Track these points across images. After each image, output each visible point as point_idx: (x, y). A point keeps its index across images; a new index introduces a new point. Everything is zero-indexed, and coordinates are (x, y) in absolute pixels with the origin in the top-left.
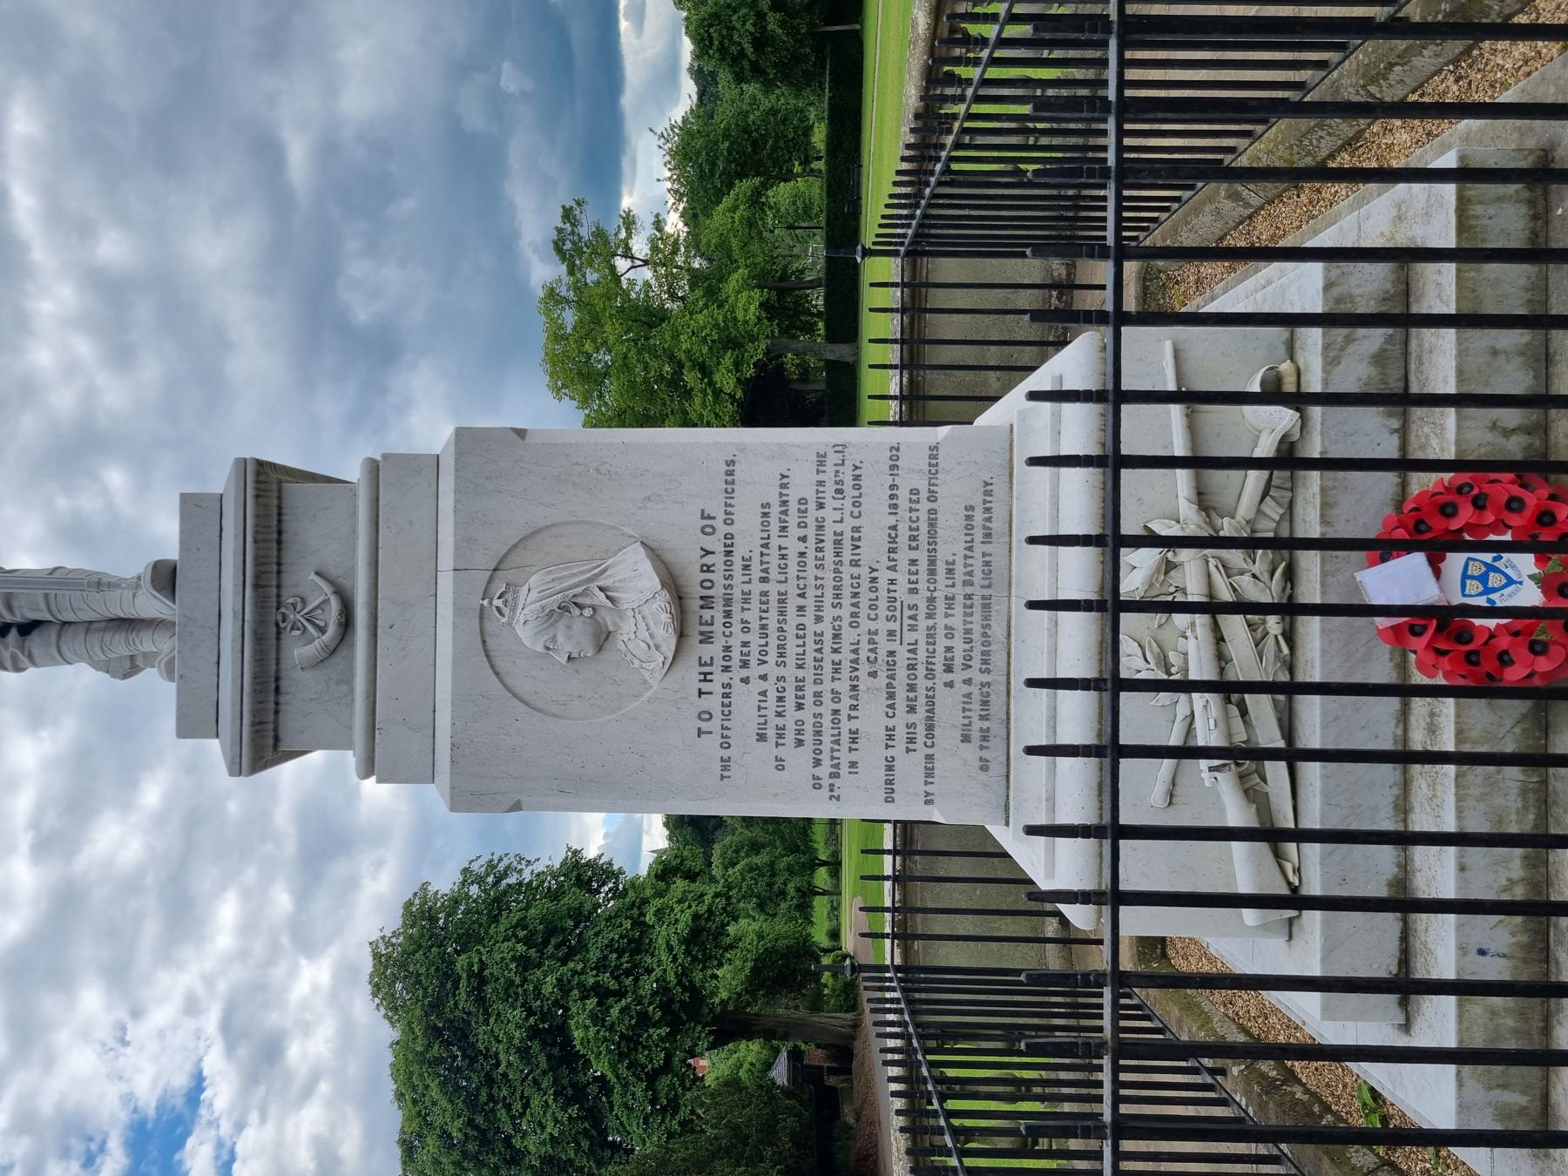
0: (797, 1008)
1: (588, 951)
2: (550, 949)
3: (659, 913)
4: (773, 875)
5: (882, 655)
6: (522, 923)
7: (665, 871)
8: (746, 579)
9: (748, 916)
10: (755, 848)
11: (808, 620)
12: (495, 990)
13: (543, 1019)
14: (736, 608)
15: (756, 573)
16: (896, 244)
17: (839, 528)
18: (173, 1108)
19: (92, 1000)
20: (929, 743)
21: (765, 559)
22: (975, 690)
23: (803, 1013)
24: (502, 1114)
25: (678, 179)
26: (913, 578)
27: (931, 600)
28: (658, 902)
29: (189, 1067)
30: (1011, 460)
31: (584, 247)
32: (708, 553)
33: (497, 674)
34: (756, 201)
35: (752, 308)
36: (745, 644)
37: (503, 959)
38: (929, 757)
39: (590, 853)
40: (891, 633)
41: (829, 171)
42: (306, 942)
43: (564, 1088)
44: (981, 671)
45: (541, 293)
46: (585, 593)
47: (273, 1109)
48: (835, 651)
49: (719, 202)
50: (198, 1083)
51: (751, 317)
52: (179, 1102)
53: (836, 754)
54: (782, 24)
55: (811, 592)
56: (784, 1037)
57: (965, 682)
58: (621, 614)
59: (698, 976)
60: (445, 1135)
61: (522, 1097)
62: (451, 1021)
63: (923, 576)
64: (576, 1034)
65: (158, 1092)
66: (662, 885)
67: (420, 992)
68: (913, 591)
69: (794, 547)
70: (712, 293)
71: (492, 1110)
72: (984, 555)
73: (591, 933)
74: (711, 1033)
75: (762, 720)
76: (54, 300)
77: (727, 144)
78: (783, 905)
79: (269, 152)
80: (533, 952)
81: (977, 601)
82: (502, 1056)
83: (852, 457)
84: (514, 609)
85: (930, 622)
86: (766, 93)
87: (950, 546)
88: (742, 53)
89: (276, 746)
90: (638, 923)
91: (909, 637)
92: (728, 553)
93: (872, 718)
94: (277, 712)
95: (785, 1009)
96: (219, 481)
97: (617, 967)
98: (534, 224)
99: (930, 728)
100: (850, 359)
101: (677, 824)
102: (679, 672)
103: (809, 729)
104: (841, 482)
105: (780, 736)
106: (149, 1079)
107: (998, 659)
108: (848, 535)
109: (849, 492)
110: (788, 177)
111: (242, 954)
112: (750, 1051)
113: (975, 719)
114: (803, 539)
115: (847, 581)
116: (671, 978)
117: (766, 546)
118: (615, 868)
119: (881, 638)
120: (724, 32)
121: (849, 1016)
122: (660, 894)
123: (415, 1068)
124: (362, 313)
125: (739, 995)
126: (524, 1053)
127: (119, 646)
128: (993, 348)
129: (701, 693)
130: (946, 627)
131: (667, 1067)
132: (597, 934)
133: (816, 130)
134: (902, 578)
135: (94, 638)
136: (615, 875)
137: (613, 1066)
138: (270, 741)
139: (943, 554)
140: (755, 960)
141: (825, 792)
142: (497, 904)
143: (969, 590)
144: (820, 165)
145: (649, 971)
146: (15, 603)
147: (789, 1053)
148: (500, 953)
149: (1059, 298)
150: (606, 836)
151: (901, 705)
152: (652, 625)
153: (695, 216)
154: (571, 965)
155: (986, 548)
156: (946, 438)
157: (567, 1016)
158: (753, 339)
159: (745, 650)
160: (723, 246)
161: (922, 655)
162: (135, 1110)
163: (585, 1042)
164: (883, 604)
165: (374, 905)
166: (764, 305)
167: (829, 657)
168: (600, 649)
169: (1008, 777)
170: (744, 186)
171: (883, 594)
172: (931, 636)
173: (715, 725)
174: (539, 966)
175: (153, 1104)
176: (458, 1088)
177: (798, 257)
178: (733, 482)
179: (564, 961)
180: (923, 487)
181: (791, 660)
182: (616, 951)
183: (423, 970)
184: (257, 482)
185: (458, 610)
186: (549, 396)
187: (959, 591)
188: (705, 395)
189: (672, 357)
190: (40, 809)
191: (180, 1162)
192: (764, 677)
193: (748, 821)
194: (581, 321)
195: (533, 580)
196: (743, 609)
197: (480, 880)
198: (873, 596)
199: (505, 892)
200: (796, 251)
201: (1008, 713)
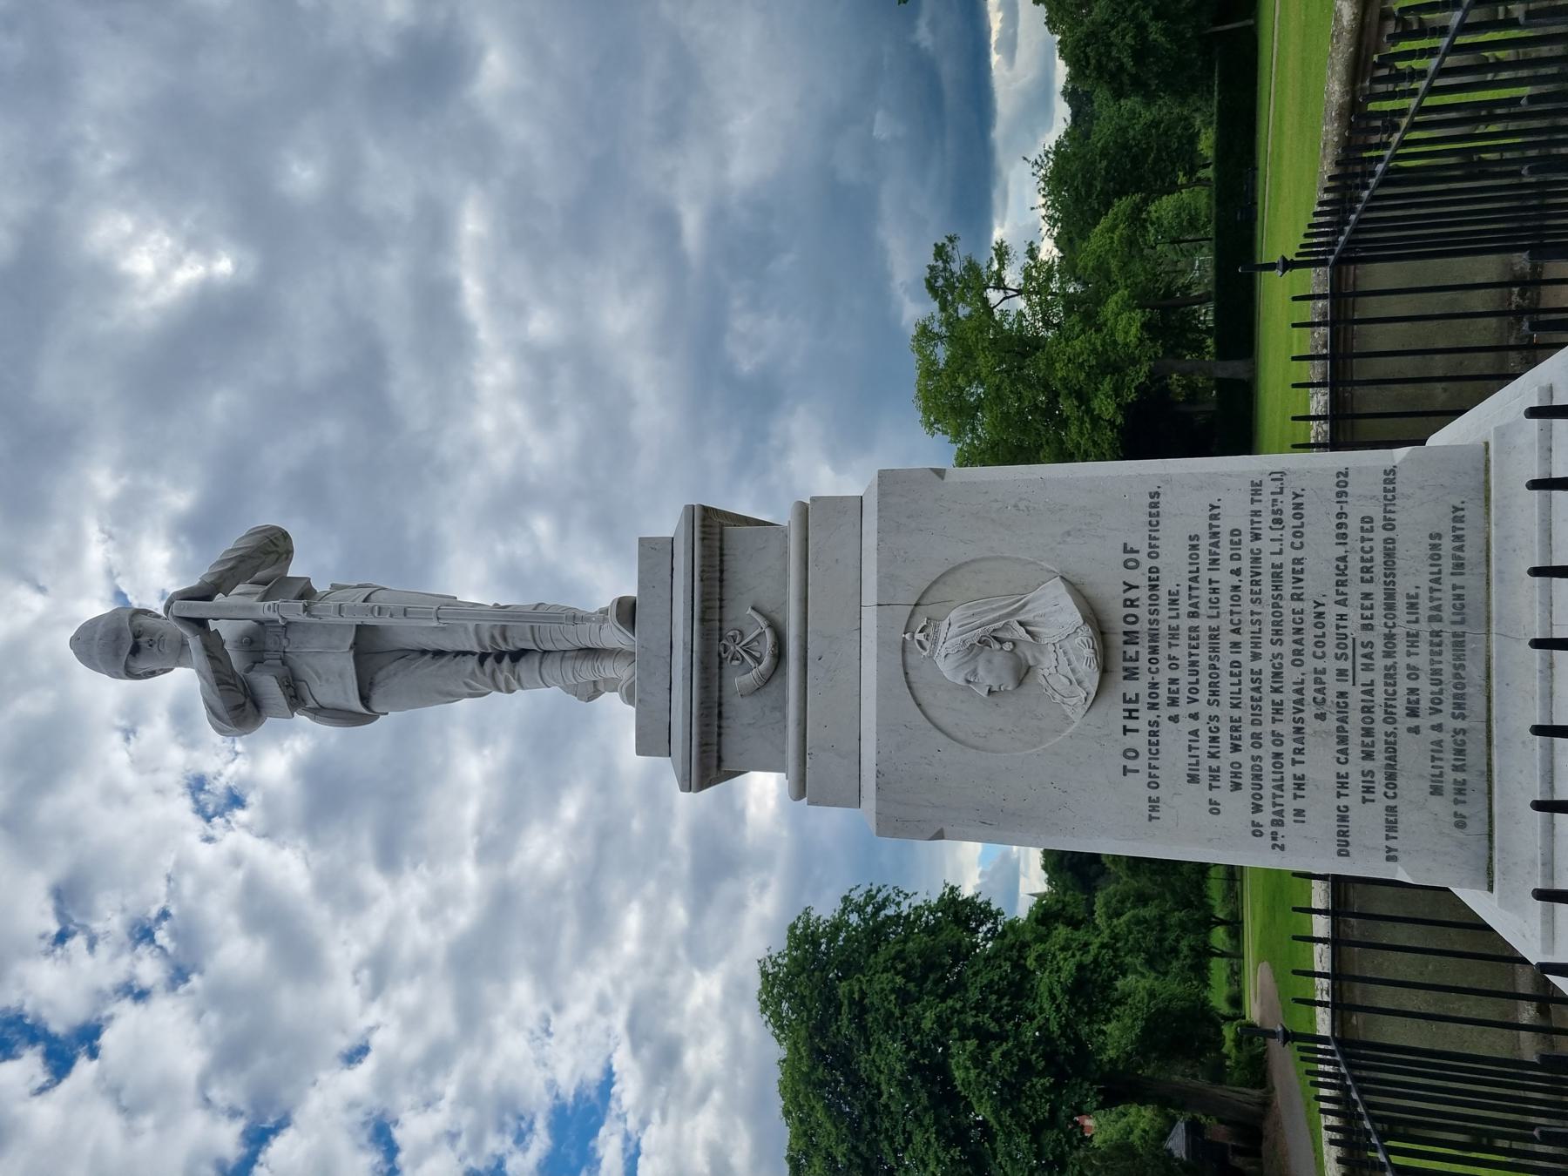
0: (1195, 1076)
1: (966, 990)
2: (929, 985)
3: (1040, 958)
4: (1164, 929)
5: (1331, 697)
6: (900, 956)
7: (1046, 915)
8: (1174, 613)
9: (1136, 972)
10: (1142, 899)
11: (1244, 656)
12: (876, 1019)
13: (925, 1053)
14: (1163, 644)
15: (1184, 606)
16: (1324, 253)
17: (1277, 560)
18: (588, 1098)
19: (522, 991)
20: (1390, 793)
21: (1194, 593)
22: (1447, 737)
23: (1202, 1082)
24: (885, 1145)
25: (1053, 205)
26: (1368, 613)
27: (1390, 637)
28: (1039, 948)
29: (601, 1061)
30: (1487, 482)
31: (956, 282)
32: (1131, 587)
33: (919, 705)
34: (1136, 218)
35: (1133, 330)
36: (1173, 681)
37: (883, 990)
38: (1391, 810)
39: (967, 892)
40: (1341, 673)
41: (1218, 178)
42: (698, 953)
43: (946, 1128)
44: (1454, 716)
45: (913, 332)
46: (1005, 627)
47: (672, 1111)
48: (1276, 690)
49: (1097, 223)
50: (609, 1078)
51: (1132, 339)
52: (593, 1093)
53: (1278, 801)
54: (1165, 32)
55: (1247, 629)
56: (1182, 1107)
57: (1433, 728)
58: (1042, 649)
59: (1084, 1030)
60: (830, 1157)
61: (904, 1131)
62: (835, 1046)
63: (1379, 611)
64: (957, 1074)
65: (577, 1080)
66: (1042, 929)
67: (805, 1014)
68: (1367, 627)
69: (1225, 579)
70: (1090, 319)
71: (875, 1140)
72: (1454, 587)
73: (970, 972)
74: (1099, 1092)
75: (1193, 761)
76: (495, 372)
77: (1104, 163)
78: (1175, 963)
79: (666, 223)
80: (911, 986)
81: (1447, 639)
82: (884, 1087)
83: (1291, 485)
84: (935, 643)
85: (1389, 662)
86: (1148, 105)
87: (1413, 575)
88: (1121, 67)
89: (719, 766)
90: (1018, 966)
91: (1363, 677)
92: (1153, 587)
93: (1320, 763)
94: (720, 735)
95: (1179, 1075)
96: (668, 523)
97: (998, 1009)
98: (906, 264)
99: (1391, 777)
100: (1245, 376)
101: (1060, 864)
102: (1102, 707)
103: (1246, 772)
104: (1280, 511)
105: (1215, 778)
106: (569, 1069)
107: (1476, 704)
108: (1288, 567)
109: (1289, 521)
110: (1173, 188)
111: (646, 962)
112: (1142, 1117)
113: (1448, 769)
114: (1237, 572)
115: (1288, 617)
116: (1054, 1027)
117: (1195, 579)
118: (994, 908)
119: (1330, 679)
120: (1102, 50)
121: (1257, 1092)
122: (1042, 939)
123: (802, 1087)
124: (746, 365)
125: (1129, 1055)
126: (905, 1086)
127: (587, 671)
128: (1438, 357)
129: (1125, 730)
130: (1409, 667)
131: (1052, 1121)
132: (975, 974)
133: (1203, 137)
134: (1354, 614)
135: (568, 665)
136: (995, 915)
137: (996, 1113)
138: (715, 762)
139: (1403, 586)
140: (1147, 1020)
141: (1267, 840)
142: (876, 933)
143: (1436, 626)
144: (1209, 173)
145: (1031, 1018)
146: (509, 634)
147: (1187, 1125)
148: (881, 983)
149: (1522, 295)
150: (981, 875)
151: (1355, 752)
152: (1073, 658)
153: (1070, 240)
154: (950, 1002)
155: (1457, 580)
156: (1405, 460)
157: (947, 1054)
158: (1134, 361)
159: (1174, 687)
160: (1102, 269)
161: (1379, 697)
162: (557, 1096)
163: (967, 1083)
164: (1331, 641)
165: (758, 926)
166: (1145, 326)
167: (1268, 697)
168: (1020, 683)
169: (1490, 836)
170: (1123, 205)
171: (1331, 630)
172: (1390, 675)
173: (1142, 763)
174: (918, 1001)
175: (572, 1093)
176: (841, 1112)
177: (1183, 272)
178: (1158, 514)
179: (943, 999)
180: (1377, 514)
181: (1225, 698)
182: (995, 993)
183: (807, 993)
184: (703, 526)
185: (882, 643)
186: (922, 431)
187: (1424, 628)
188: (1083, 423)
189: (1046, 386)
190: (483, 817)
191: (594, 1149)
192: (1195, 716)
193: (1136, 865)
194: (953, 355)
195: (953, 615)
196: (1170, 645)
197: (860, 909)
198: (1319, 632)
199: (884, 923)
200: (1180, 266)
201: (1489, 765)
